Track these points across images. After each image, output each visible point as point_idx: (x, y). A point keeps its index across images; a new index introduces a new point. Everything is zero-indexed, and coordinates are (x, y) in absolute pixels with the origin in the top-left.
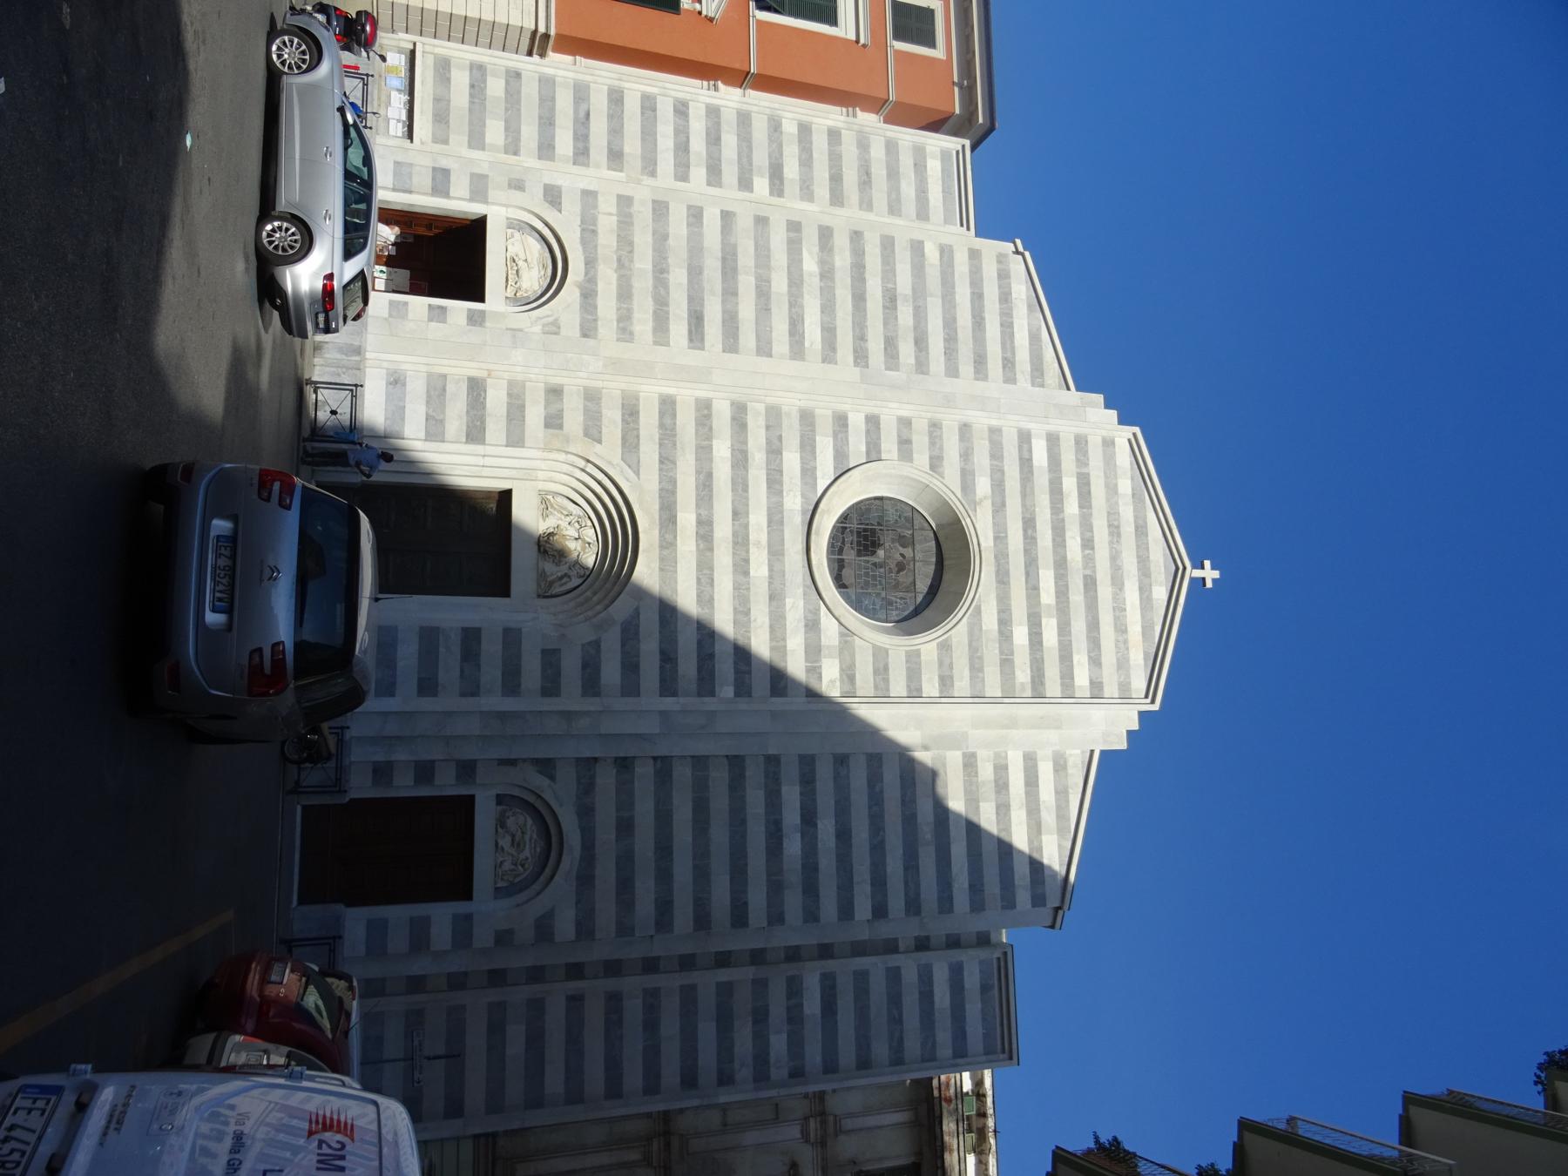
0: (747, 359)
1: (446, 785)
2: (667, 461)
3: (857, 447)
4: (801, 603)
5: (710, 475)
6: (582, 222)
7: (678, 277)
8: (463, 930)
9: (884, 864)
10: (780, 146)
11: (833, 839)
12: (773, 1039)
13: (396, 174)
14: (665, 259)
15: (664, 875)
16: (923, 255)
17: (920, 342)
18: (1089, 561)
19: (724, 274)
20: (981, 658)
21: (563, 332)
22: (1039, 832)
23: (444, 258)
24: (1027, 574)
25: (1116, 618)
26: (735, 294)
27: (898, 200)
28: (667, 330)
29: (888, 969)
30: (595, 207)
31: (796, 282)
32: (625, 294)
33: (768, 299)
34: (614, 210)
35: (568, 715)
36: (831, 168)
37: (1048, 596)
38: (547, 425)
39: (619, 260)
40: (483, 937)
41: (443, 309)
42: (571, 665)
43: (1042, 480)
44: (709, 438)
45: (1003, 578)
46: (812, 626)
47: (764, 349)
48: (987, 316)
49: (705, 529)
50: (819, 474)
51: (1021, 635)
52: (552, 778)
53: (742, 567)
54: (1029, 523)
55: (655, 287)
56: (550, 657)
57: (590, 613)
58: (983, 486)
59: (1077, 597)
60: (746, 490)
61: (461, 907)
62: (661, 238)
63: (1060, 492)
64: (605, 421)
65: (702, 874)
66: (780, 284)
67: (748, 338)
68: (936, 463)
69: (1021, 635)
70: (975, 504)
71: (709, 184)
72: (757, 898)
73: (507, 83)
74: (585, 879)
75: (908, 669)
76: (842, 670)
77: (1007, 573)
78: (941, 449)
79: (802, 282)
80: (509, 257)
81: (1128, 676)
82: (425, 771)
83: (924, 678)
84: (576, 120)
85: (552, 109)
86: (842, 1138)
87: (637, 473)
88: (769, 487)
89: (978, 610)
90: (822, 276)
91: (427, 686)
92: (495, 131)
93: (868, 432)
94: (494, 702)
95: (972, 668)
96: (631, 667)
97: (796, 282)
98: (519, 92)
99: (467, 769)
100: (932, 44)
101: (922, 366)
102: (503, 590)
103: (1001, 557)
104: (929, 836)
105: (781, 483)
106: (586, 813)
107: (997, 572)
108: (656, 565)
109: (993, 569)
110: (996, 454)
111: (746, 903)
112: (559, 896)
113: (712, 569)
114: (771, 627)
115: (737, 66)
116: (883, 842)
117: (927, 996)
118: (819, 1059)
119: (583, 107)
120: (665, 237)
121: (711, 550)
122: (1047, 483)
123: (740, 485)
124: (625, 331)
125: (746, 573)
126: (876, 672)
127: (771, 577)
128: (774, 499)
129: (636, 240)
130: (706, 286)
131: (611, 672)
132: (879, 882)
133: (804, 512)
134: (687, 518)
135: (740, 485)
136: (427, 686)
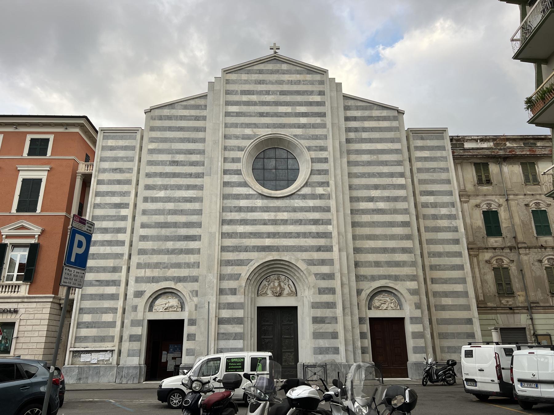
0: (204, 219)
1: (366, 328)
2: (246, 249)
3: (235, 178)
4: (296, 201)
5: (251, 233)
6: (149, 282)
7: (170, 245)
8: (414, 320)
9: (385, 173)
10: (106, 204)
11: (378, 191)
12: (442, 213)
13: (133, 356)
14: (163, 250)
15: (393, 250)
16: (154, 149)
17: (191, 152)
18: (274, 93)
19: (168, 227)
20: (313, 135)
21: (196, 289)
22: (372, 117)
23: (165, 337)
24: (281, 117)
25: (295, 84)
26: (176, 223)
27: (127, 158)
28: (192, 249)
29: (418, 172)
30: (142, 277)
31: (169, 200)
32: (178, 266)
33: (177, 210)
34: (143, 270)
35: (342, 285)
36: (114, 184)
37: (289, 109)
38: (235, 294)
39: (164, 268)
40: (417, 313)
41: (189, 335)
42: (324, 284)
43: (244, 109)
44: (237, 233)
45: (283, 126)
46: (304, 197)
47: (199, 212)
48: (178, 126)
49: (270, 235)
50: (248, 193)
51: (303, 120)
52: (362, 290)
53: (285, 222)
54: (261, 115)
55: (175, 254)
56: (322, 291)
57: (304, 277)
58: (248, 131)
59: (288, 98)
60: (255, 220)
61: (407, 323)
62: (154, 252)
63: (248, 102)
64: (232, 272)
65: (393, 237)
66: (170, 206)
67: (194, 218)
68: (240, 149)
69: (303, 120)
70: (255, 135)
71: (125, 233)
72: (400, 218)
73: (85, 313)
74: (396, 278)
75: (318, 162)
76: (320, 186)
77: (280, 124)
78: (235, 146)
79: (169, 197)
80: (163, 311)
81: (316, 81)
82: (363, 335)
83: (321, 157)
84: (99, 285)
85: (96, 295)
86: (467, 189)
87: (252, 260)
88: (254, 212)
89: (295, 136)
90: (166, 189)
91: (334, 335)
92: (107, 318)
93: (230, 174)
94: (339, 311)
95: (316, 139)
96: (323, 262)
97: (169, 200)
98: (89, 308)
99: (361, 320)
100: (48, 140)
101: (202, 152)
102: (294, 309)
103: (275, 126)
104: (375, 157)
105: (252, 207)
106: (373, 278)
107: (281, 128)
108: (286, 253)
109: (280, 130)
110: (236, 125)
111: (402, 222)
112: (402, 287)
113: (286, 233)
114: (306, 212)
115: (63, 220)
116: (378, 173)
117: (426, 159)
118: (448, 197)
119: (94, 283)
120: (153, 250)
121: (279, 233)
122: (245, 107)
123: (254, 222)
124: (197, 265)
125: (287, 220)
126: (320, 174)
127: (287, 211)
128: (258, 210)
129: (155, 261)
130: (173, 234)
131: (325, 269)
132: (392, 175)
133: (262, 199)
134: (268, 242)
135: (254, 222)
136: (334, 335)
